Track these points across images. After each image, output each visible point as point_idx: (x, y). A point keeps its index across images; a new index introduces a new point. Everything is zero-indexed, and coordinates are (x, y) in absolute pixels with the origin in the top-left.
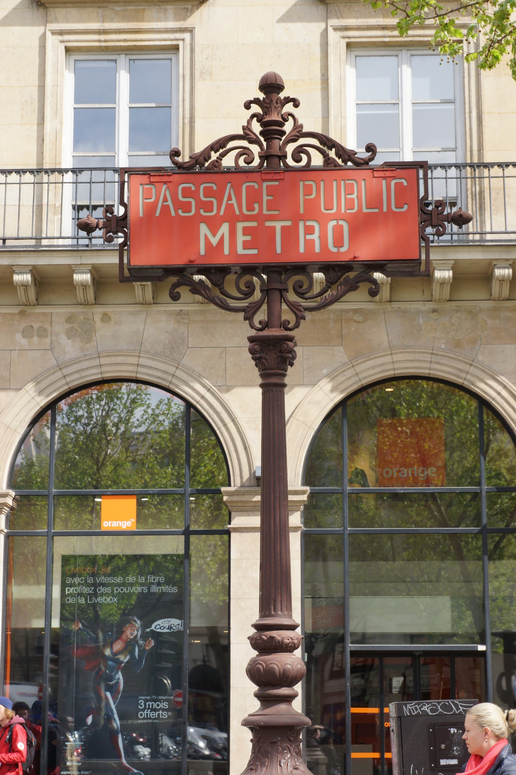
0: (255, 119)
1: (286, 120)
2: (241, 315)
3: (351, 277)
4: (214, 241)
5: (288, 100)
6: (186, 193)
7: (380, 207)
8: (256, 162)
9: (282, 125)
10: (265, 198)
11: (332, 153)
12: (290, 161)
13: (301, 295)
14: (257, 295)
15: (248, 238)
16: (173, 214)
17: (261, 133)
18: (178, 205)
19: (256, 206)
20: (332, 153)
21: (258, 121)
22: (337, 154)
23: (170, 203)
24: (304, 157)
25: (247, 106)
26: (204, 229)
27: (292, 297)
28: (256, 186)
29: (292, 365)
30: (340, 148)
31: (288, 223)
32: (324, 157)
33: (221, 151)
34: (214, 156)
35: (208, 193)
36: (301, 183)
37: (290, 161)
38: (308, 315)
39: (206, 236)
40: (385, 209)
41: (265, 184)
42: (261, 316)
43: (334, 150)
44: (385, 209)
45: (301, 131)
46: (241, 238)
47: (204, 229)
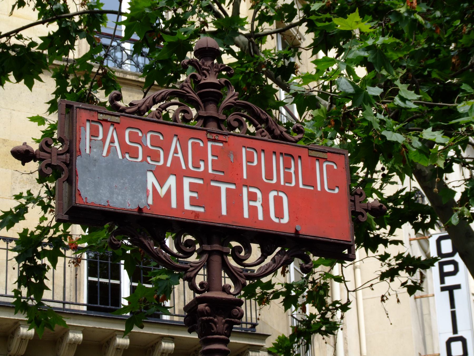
4: (162, 192)
7: (315, 186)
44: (319, 189)
46: (187, 194)
47: (151, 179)
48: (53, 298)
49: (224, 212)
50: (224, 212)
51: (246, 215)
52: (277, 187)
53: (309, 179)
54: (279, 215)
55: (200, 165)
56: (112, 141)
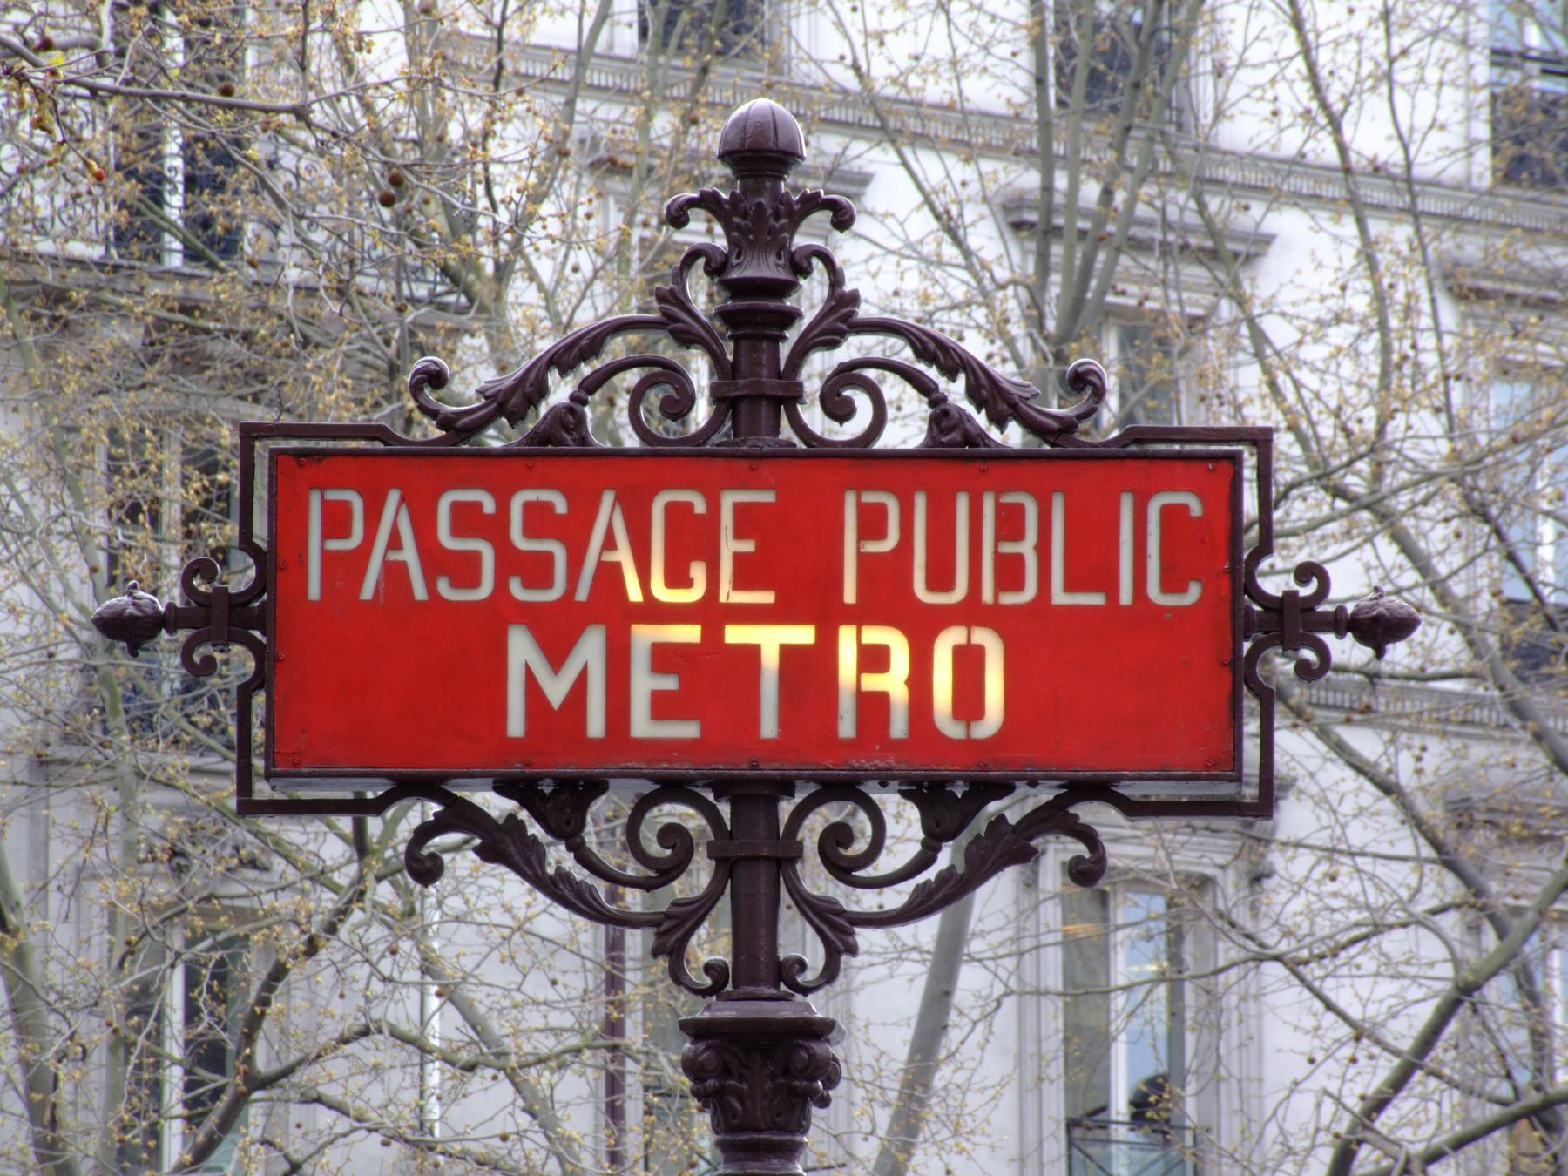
0: (701, 261)
1: (806, 272)
2: (865, 311)
3: (1013, 817)
4: (556, 690)
5: (812, 203)
6: (466, 519)
7: (1112, 589)
8: (701, 413)
9: (787, 288)
10: (730, 546)
11: (955, 391)
12: (814, 417)
13: (843, 870)
14: (699, 876)
15: (670, 683)
16: (420, 593)
17: (724, 315)
18: (435, 561)
19: (698, 572)
20: (955, 391)
21: (711, 271)
22: (973, 393)
23: (409, 554)
24: (862, 403)
25: (677, 218)
26: (521, 648)
27: (816, 879)
28: (700, 507)
29: (824, 1102)
30: (984, 381)
31: (804, 635)
32: (932, 404)
33: (586, 370)
34: (561, 391)
35: (538, 520)
36: (850, 502)
37: (814, 417)
38: (865, 937)
39: (530, 678)
40: (1126, 596)
41: (729, 499)
42: (711, 945)
43: (962, 378)
44: (1126, 596)
45: (852, 313)
46: (643, 684)
47: (521, 648)
48: (1396, 1053)
49: (769, 727)
50: (769, 727)
51: (847, 728)
52: (971, 613)
53: (1090, 567)
54: (968, 700)
55: (1183, 589)
56: (395, 542)
